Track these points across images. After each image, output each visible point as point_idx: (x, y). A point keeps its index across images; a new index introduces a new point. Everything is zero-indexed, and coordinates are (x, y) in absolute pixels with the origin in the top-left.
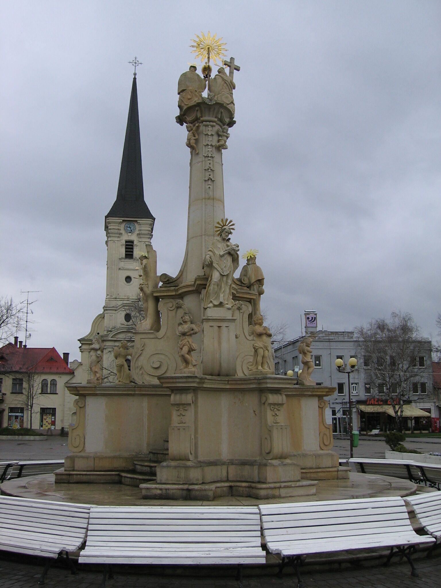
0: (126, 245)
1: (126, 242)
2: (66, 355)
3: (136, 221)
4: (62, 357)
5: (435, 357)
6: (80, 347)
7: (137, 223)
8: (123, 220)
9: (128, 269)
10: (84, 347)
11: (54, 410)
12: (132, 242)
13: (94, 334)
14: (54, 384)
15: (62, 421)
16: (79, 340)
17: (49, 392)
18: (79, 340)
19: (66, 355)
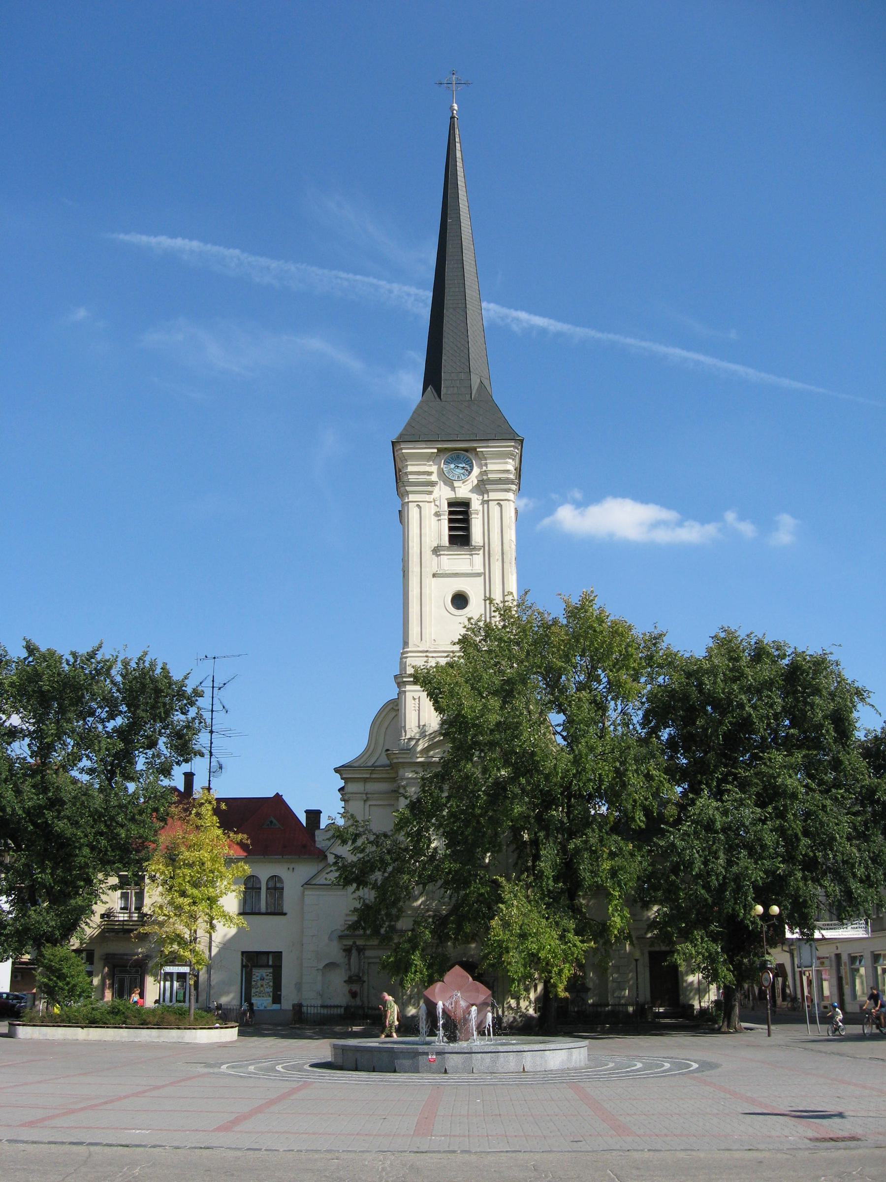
0: (450, 513)
1: (450, 504)
2: (314, 815)
3: (475, 449)
4: (303, 818)
5: (867, 723)
6: (341, 790)
7: (477, 453)
8: (439, 450)
9: (456, 575)
10: (352, 788)
11: (278, 955)
12: (466, 504)
13: (379, 751)
14: (275, 888)
15: (299, 986)
16: (337, 770)
17: (263, 910)
18: (337, 770)
19: (314, 815)
